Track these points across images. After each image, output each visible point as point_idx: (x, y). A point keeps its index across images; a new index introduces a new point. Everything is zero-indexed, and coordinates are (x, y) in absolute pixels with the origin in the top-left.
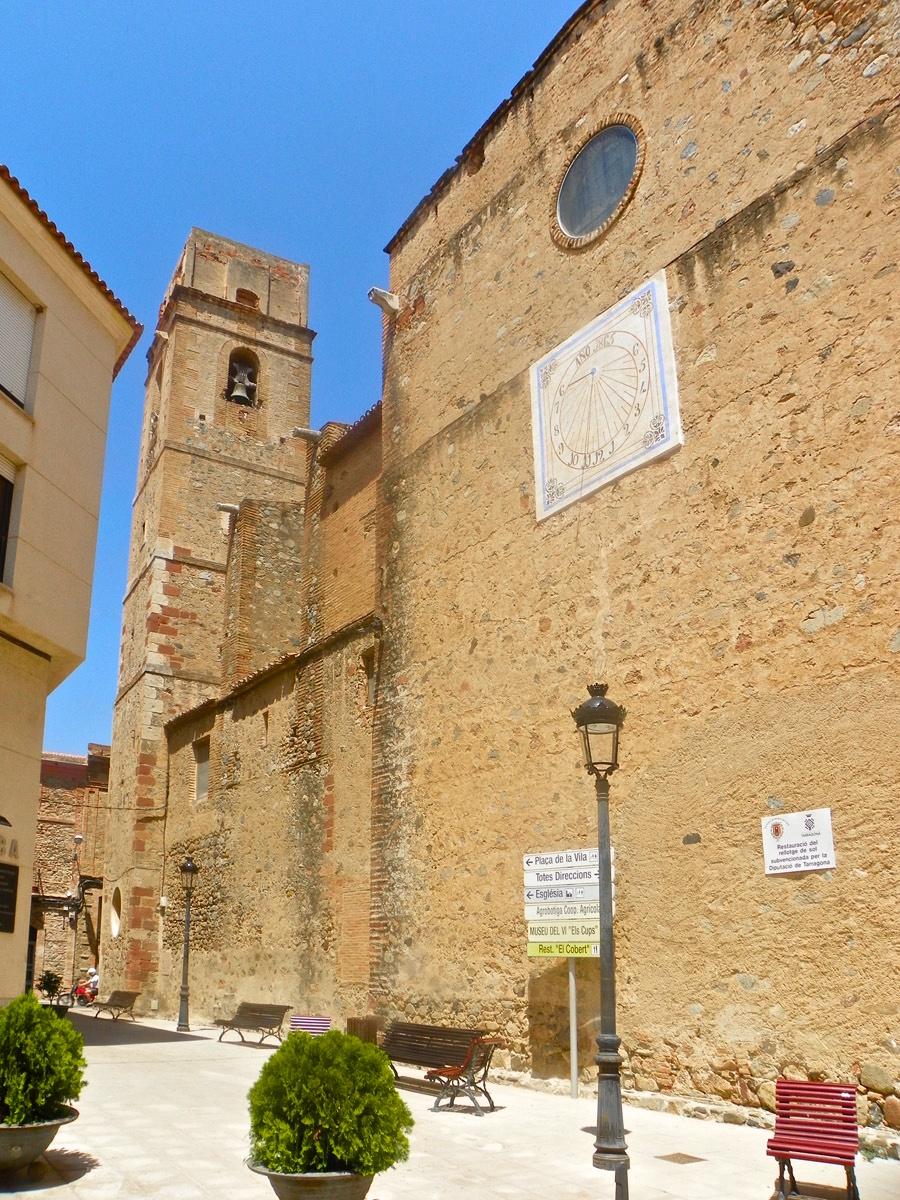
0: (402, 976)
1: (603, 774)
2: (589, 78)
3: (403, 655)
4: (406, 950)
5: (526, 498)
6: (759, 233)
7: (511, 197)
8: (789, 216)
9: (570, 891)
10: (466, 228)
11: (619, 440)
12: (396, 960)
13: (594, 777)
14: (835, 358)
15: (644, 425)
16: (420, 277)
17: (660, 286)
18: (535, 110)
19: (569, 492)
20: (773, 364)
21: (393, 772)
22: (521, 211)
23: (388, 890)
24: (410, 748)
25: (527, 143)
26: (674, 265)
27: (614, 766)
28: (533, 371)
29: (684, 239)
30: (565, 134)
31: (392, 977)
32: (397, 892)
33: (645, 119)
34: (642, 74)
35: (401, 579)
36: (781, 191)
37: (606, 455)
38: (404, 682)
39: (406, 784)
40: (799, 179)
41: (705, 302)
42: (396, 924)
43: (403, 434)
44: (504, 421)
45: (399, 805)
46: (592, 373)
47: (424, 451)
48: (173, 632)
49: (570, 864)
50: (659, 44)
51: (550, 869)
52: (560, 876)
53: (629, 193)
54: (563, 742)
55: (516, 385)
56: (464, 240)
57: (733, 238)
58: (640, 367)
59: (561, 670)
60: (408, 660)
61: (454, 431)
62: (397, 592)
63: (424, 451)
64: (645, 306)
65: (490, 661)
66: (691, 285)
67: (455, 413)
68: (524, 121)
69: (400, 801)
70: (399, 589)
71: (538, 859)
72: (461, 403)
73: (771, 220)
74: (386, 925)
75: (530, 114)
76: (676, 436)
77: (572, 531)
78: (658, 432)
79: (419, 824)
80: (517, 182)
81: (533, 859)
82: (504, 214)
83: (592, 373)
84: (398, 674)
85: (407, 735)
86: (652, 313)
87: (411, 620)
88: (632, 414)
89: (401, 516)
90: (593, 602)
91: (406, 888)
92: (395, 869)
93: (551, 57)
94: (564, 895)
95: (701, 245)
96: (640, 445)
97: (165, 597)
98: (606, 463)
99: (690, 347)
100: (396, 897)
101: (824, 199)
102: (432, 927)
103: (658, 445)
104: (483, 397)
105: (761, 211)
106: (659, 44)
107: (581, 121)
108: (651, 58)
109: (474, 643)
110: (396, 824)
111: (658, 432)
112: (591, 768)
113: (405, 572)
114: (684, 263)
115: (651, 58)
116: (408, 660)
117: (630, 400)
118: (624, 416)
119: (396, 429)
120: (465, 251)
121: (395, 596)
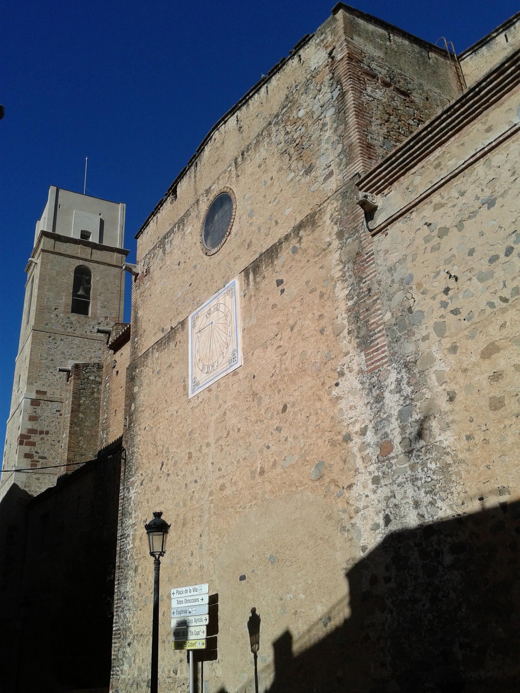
0: (126, 667)
1: (157, 556)
2: (218, 163)
3: (133, 469)
4: (128, 650)
5: (185, 388)
6: (272, 262)
7: (185, 222)
8: (284, 255)
9: (190, 610)
10: (167, 234)
11: (220, 360)
12: (124, 656)
13: (154, 559)
14: (295, 330)
15: (229, 355)
16: (149, 256)
17: (237, 282)
18: (197, 175)
19: (202, 384)
20: (275, 329)
21: (126, 538)
22: (189, 230)
23: (122, 612)
24: (134, 524)
25: (194, 193)
26: (243, 272)
27: (162, 553)
28: (190, 319)
29: (247, 259)
30: (208, 192)
31: (121, 668)
32: (126, 612)
33: (238, 193)
34: (236, 168)
35: (134, 425)
36: (280, 243)
37: (215, 367)
38: (133, 483)
39: (131, 546)
40: (287, 238)
41: (253, 293)
42: (124, 632)
43: (139, 342)
44: (178, 343)
45: (128, 559)
46: (212, 323)
47: (146, 355)
48: (33, 444)
49: (190, 594)
50: (243, 154)
51: (183, 597)
52: (187, 601)
53: (229, 230)
54: (196, 522)
55: (183, 323)
56: (166, 240)
57: (263, 263)
58: (229, 324)
59: (196, 482)
60: (135, 473)
61: (161, 344)
62: (132, 433)
63: (146, 355)
64: (231, 292)
65: (168, 475)
66: (248, 284)
67: (161, 335)
68: (193, 179)
69: (129, 556)
70: (133, 431)
71: (177, 591)
72: (163, 330)
73: (277, 257)
74: (119, 634)
75: (195, 177)
76: (240, 361)
77: (202, 405)
78: (234, 359)
79: (136, 570)
80: (187, 214)
81: (175, 592)
82: (183, 230)
83: (212, 323)
84: (131, 480)
85: (133, 516)
86: (234, 297)
87: (137, 449)
88: (225, 348)
89: (136, 389)
90: (208, 445)
91: (129, 610)
92: (125, 598)
93: (204, 148)
94: (188, 612)
95: (252, 265)
96: (228, 364)
97: (29, 422)
98: (216, 371)
99: (247, 312)
100: (125, 615)
101: (295, 250)
102: (140, 634)
103: (234, 365)
104: (172, 328)
105: (272, 253)
106: (243, 154)
107: (214, 186)
108: (240, 159)
109: (162, 465)
110: (126, 570)
111: (234, 359)
112: (152, 554)
113: (136, 421)
114: (246, 271)
115: (240, 159)
116: (135, 473)
117: (225, 341)
118: (222, 348)
119: (136, 339)
120: (167, 247)
121: (131, 435)
